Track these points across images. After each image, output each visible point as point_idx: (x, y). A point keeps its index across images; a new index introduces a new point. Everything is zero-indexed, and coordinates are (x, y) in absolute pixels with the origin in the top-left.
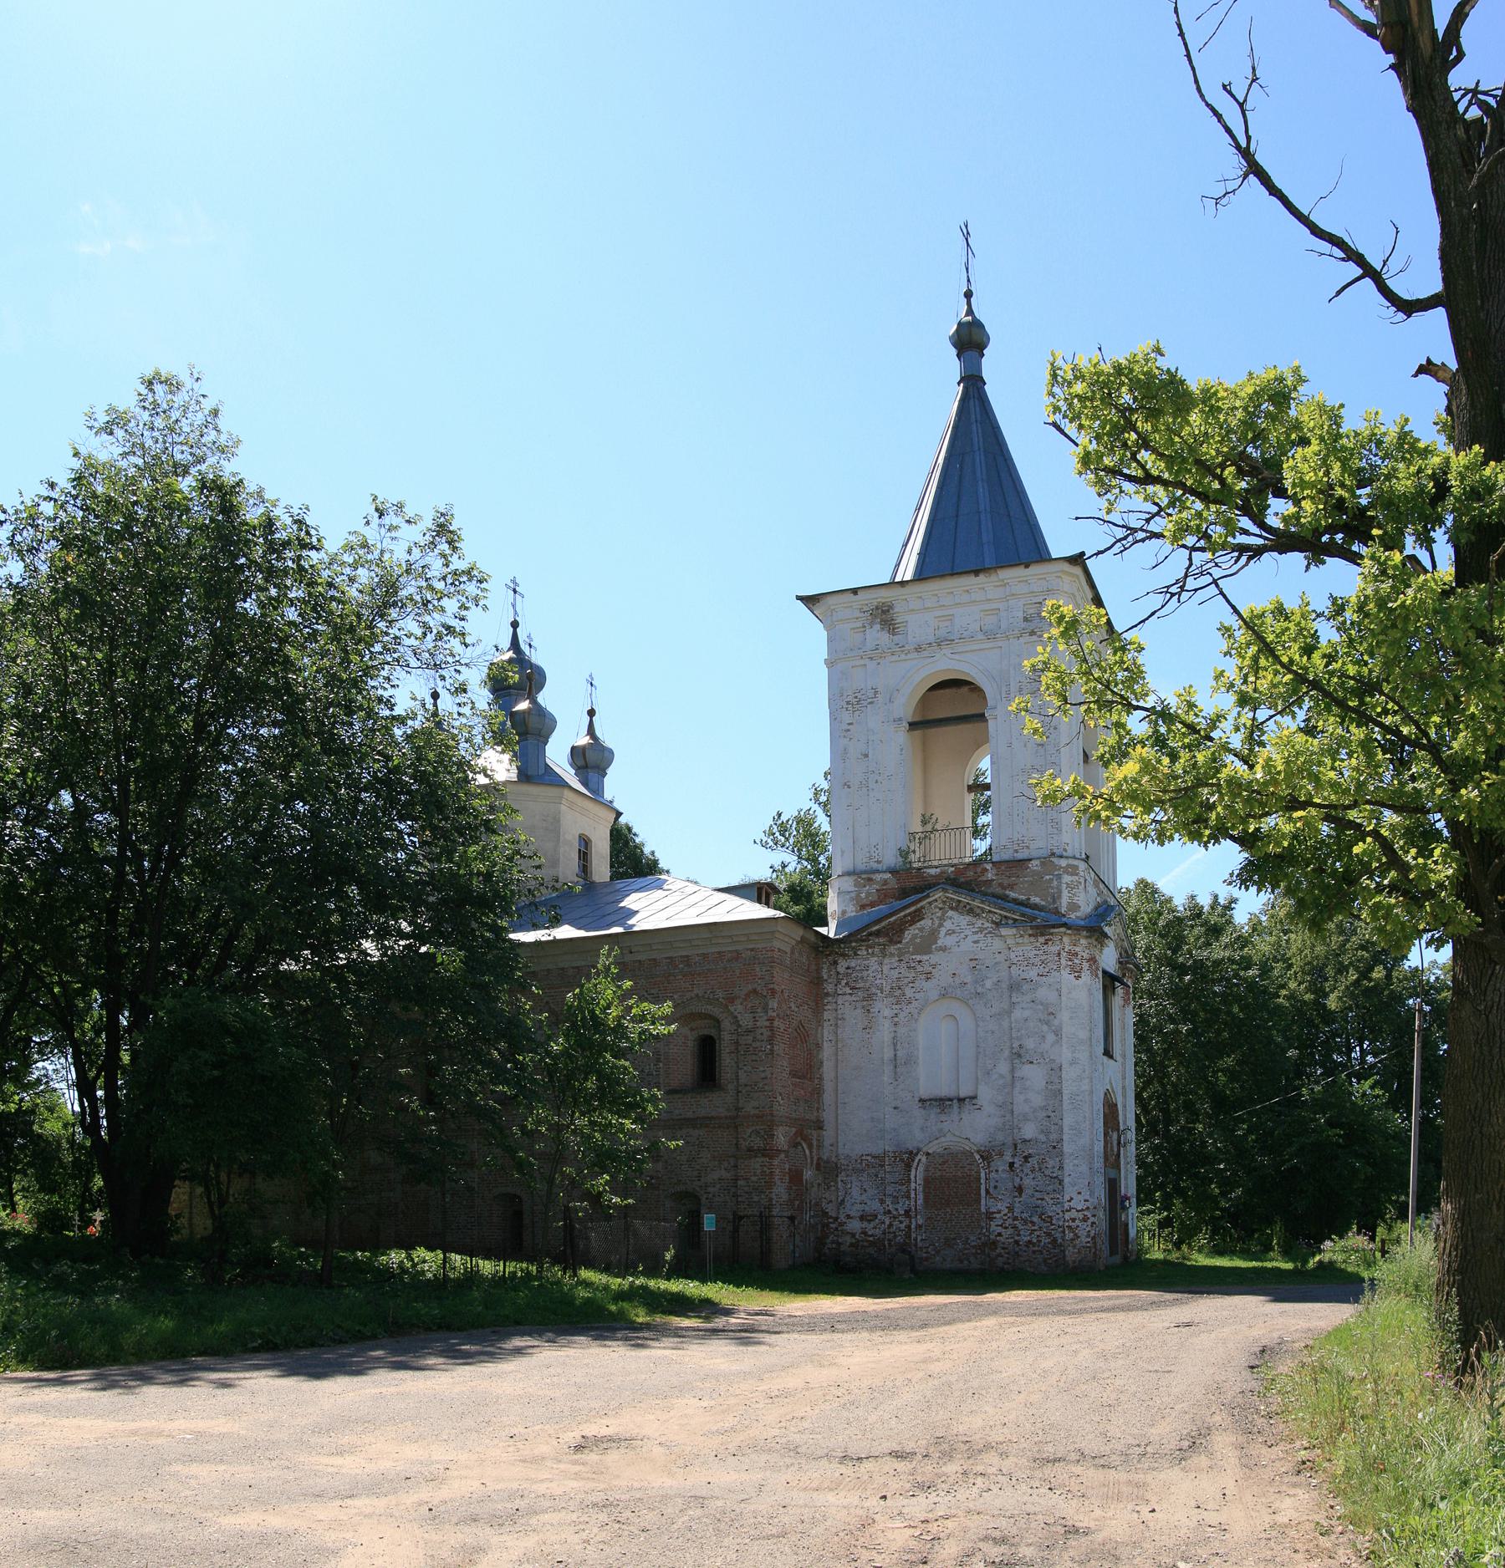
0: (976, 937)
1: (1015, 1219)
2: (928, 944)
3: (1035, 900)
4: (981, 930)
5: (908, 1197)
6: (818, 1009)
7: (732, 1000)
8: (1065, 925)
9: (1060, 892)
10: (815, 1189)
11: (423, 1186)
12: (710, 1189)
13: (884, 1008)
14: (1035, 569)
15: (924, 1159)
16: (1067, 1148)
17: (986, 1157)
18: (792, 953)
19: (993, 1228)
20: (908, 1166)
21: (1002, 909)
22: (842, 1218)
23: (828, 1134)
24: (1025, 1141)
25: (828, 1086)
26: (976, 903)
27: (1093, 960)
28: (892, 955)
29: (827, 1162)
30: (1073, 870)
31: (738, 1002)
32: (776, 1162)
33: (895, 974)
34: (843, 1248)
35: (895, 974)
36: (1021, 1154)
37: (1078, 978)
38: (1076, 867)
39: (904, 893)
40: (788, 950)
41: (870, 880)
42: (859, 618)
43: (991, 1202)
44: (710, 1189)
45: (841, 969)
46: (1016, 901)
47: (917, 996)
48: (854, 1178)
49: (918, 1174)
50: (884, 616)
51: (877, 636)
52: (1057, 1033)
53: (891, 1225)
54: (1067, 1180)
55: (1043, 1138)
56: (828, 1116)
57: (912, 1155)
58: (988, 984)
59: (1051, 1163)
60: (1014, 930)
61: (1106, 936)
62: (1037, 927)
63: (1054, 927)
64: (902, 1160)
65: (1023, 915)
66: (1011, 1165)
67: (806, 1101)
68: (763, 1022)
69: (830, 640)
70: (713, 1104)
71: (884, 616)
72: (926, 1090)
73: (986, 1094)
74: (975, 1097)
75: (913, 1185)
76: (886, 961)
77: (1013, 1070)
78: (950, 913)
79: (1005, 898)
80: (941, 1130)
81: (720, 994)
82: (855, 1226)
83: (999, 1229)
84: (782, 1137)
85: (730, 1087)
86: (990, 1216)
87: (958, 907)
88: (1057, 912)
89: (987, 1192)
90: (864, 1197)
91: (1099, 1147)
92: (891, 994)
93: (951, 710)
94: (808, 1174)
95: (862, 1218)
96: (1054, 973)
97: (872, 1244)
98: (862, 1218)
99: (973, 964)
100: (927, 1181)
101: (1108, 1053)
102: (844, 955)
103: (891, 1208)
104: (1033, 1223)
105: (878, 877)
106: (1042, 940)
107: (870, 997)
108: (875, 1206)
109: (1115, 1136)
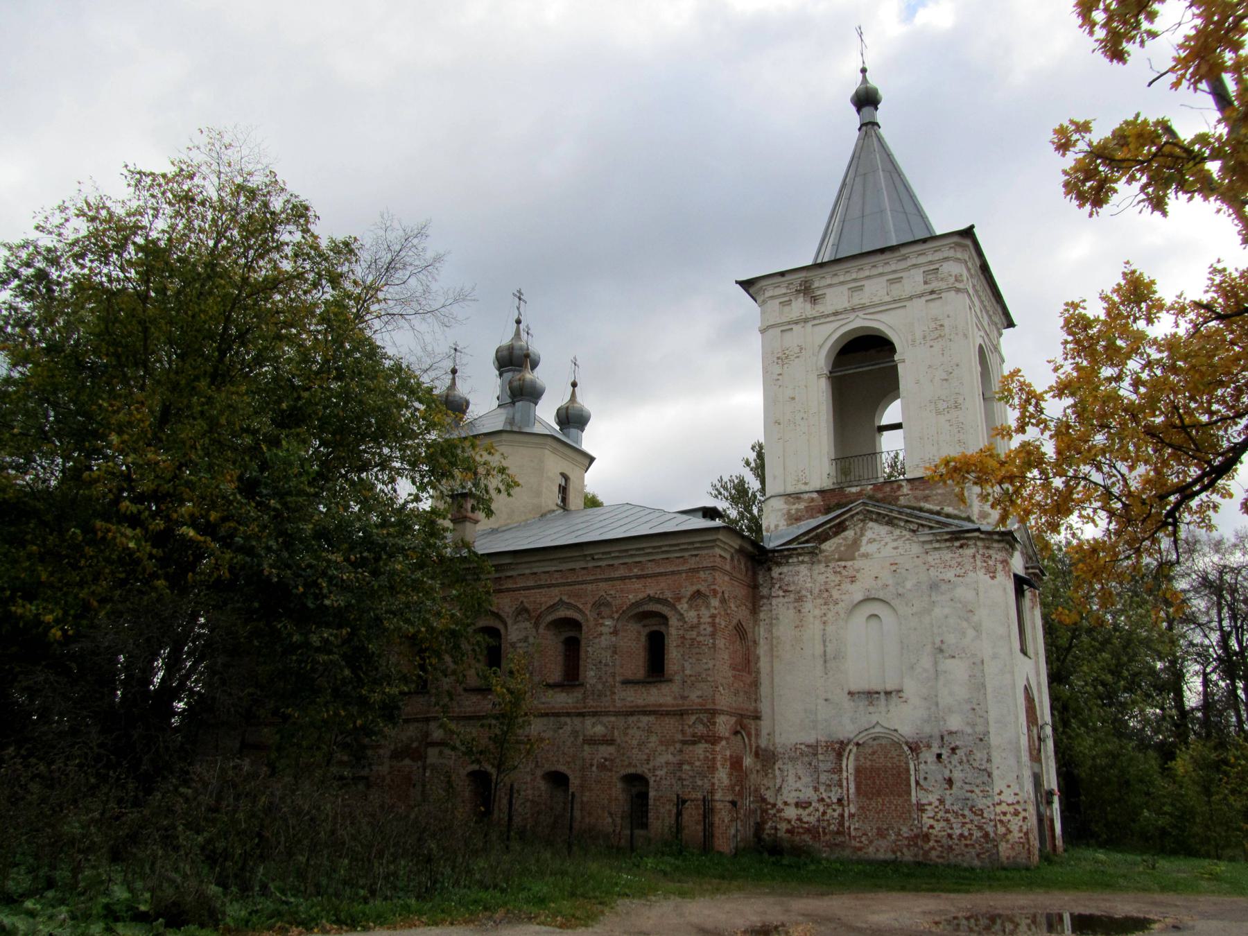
0: (895, 544)
1: (947, 811)
5: (841, 786)
6: (755, 610)
12: (658, 773)
13: (811, 608)
15: (855, 749)
16: (994, 740)
19: (925, 819)
20: (839, 755)
21: (919, 518)
22: (780, 805)
23: (765, 725)
24: (951, 733)
29: (766, 750)
31: (685, 600)
32: (718, 749)
33: (822, 579)
35: (822, 579)
37: (993, 578)
41: (799, 498)
43: (921, 794)
44: (658, 773)
47: (844, 597)
49: (849, 764)
52: (977, 628)
53: (824, 813)
54: (995, 773)
56: (764, 708)
58: (909, 585)
59: (978, 755)
64: (834, 749)
66: (939, 756)
75: (845, 774)
77: (936, 663)
78: (871, 524)
79: (921, 510)
82: (791, 813)
83: (931, 822)
84: (724, 725)
85: (677, 678)
86: (921, 808)
88: (969, 519)
89: (917, 783)
90: (799, 785)
91: (1024, 741)
94: (748, 761)
95: (797, 805)
96: (971, 574)
97: (808, 831)
99: (894, 568)
100: (858, 771)
103: (824, 795)
105: (806, 496)
107: (800, 599)
108: (808, 794)
109: (1035, 731)
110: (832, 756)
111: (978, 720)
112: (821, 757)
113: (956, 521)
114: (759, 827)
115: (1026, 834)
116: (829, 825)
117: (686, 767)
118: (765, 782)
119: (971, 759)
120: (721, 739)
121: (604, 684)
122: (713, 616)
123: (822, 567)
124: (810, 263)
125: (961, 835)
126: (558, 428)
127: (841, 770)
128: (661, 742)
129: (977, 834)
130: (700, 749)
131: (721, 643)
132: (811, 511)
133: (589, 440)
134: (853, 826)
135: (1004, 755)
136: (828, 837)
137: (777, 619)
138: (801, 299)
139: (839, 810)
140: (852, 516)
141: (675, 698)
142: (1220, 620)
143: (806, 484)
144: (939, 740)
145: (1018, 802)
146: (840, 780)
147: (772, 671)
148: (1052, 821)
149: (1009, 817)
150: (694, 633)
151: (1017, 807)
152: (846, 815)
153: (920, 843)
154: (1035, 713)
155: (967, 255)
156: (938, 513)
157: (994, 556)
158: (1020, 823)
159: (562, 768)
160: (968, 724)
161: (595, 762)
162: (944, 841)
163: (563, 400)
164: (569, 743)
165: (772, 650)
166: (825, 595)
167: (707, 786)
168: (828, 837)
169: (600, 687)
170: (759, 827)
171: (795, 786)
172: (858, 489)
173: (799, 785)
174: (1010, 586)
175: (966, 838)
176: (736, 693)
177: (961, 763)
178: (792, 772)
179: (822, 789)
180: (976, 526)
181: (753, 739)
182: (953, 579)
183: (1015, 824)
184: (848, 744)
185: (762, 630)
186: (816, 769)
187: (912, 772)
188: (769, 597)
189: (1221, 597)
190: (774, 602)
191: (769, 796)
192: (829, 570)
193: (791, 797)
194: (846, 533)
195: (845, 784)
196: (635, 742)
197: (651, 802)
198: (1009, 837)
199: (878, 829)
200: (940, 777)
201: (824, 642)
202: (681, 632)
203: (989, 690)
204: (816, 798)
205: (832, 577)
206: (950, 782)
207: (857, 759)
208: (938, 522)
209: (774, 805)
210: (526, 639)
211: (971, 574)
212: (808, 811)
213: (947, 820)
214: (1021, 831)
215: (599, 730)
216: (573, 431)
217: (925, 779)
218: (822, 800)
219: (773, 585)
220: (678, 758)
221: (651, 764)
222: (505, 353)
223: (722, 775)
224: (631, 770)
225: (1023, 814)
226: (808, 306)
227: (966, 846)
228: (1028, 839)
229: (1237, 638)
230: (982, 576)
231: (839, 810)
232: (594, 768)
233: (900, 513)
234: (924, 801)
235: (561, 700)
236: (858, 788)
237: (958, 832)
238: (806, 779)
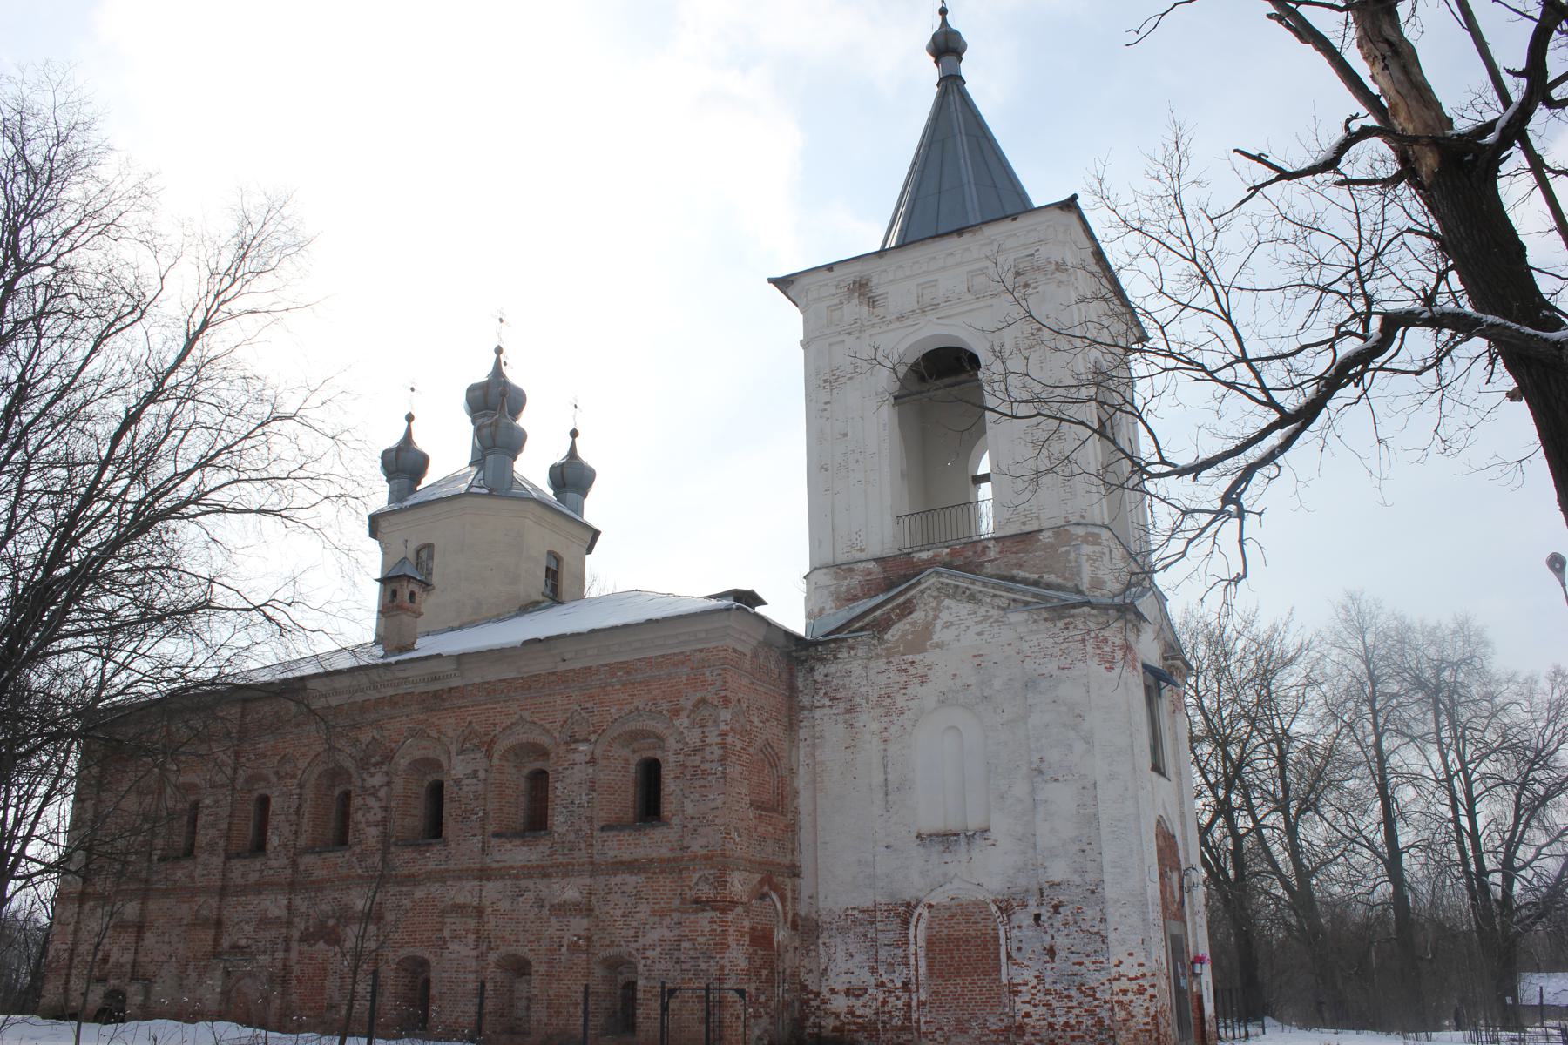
0: (979, 628)
1: (1048, 993)
2: (920, 641)
3: (1050, 578)
4: (986, 618)
5: (907, 964)
6: (791, 727)
7: (676, 712)
8: (1088, 603)
9: (1079, 567)
10: (790, 954)
11: (321, 945)
12: (649, 953)
13: (869, 722)
14: (1023, 222)
15: (925, 913)
16: (1110, 891)
17: (1006, 908)
18: (755, 656)
19: (1019, 1006)
20: (905, 923)
21: (1010, 590)
22: (825, 993)
23: (805, 884)
24: (1052, 885)
25: (805, 821)
26: (977, 587)
27: (1128, 648)
28: (878, 656)
29: (806, 919)
30: (1094, 540)
31: (684, 714)
32: (730, 918)
33: (883, 679)
34: (825, 1033)
35: (883, 679)
36: (1049, 903)
37: (1110, 669)
38: (1098, 536)
39: (889, 585)
40: (747, 651)
41: (851, 570)
42: (828, 294)
43: (1014, 970)
44: (649, 953)
45: (818, 676)
46: (1025, 581)
47: (911, 704)
48: (839, 940)
49: (919, 933)
50: (861, 289)
51: (855, 309)
52: (1088, 740)
53: (884, 1003)
54: (1112, 936)
55: (1077, 879)
56: (805, 860)
57: (910, 907)
58: (997, 683)
59: (1089, 913)
60: (1025, 615)
61: (1140, 616)
62: (1053, 609)
63: (1074, 606)
64: (897, 915)
65: (1035, 595)
66: (1037, 917)
67: (777, 840)
68: (713, 738)
69: (806, 322)
70: (654, 844)
71: (861, 289)
72: (932, 822)
73: (1001, 826)
74: (987, 830)
75: (912, 948)
76: (873, 664)
77: (1033, 790)
78: (947, 602)
79: (1013, 579)
80: (945, 875)
81: (664, 705)
82: (840, 1003)
83: (1028, 1008)
84: (739, 885)
85: (675, 821)
86: (1014, 990)
87: (957, 593)
88: (1079, 592)
89: (1009, 956)
90: (850, 965)
91: (1154, 890)
92: (878, 704)
93: (943, 380)
94: (781, 935)
95: (848, 993)
96: (1079, 665)
97: (862, 1027)
98: (848, 993)
99: (977, 661)
100: (931, 942)
101: (1157, 768)
102: (822, 660)
103: (885, 978)
104: (1069, 998)
105: (861, 566)
106: (1061, 624)
107: (852, 709)
108: (864, 977)
109: (1175, 877)
110: (895, 924)
111: (1090, 864)
112: (880, 926)
113: (1060, 594)
114: (799, 1023)
115: (1154, 1018)
116: (891, 1018)
117: (685, 945)
118: (806, 962)
119: (1079, 918)
120: (735, 904)
121: (576, 832)
122: (723, 734)
123: (881, 664)
124: (878, 248)
125: (1066, 1024)
126: (550, 492)
127: (907, 942)
128: (654, 913)
129: (1088, 1021)
130: (705, 919)
131: (735, 771)
132: (870, 589)
133: (594, 509)
134: (921, 1018)
135: (1124, 911)
136: (889, 1036)
137: (822, 737)
138: (855, 301)
139: (905, 997)
140: (922, 592)
141: (672, 850)
142: (1438, 730)
143: (862, 550)
144: (1037, 897)
145: (1144, 975)
146: (906, 956)
147: (815, 810)
148: (1200, 998)
149: (1130, 996)
150: (697, 760)
151: (1141, 982)
152: (914, 1004)
153: (1012, 1037)
154: (1176, 854)
155: (1074, 218)
156: (1036, 583)
157: (1111, 639)
158: (1146, 1004)
159: (522, 951)
160: (1076, 871)
161: (565, 942)
162: (1044, 1033)
163: (559, 455)
164: (531, 916)
165: (814, 781)
166: (887, 702)
167: (714, 971)
168: (889, 1036)
169: (572, 836)
170: (799, 1023)
171: (845, 967)
172: (931, 553)
173: (850, 965)
174: (1136, 683)
175: (1072, 1028)
176: (762, 840)
177: (1066, 925)
178: (841, 948)
179: (882, 969)
180: (1085, 599)
181: (789, 904)
182: (1055, 673)
183: (1139, 1005)
184: (916, 906)
185: (802, 753)
186: (874, 941)
187: (1002, 941)
188: (812, 708)
189: (1437, 701)
190: (818, 714)
191: (811, 981)
192: (893, 667)
193: (840, 983)
194: (914, 615)
195: (912, 962)
196: (619, 912)
197: (640, 995)
198: (1131, 1024)
199: (958, 1020)
200: (1038, 947)
201: (885, 766)
202: (681, 758)
203: (1103, 824)
204: (873, 982)
205: (895, 677)
206: (1051, 952)
207: (929, 928)
208: (1035, 595)
209: (818, 994)
210: (475, 774)
211: (1079, 665)
212: (861, 1001)
213: (1048, 1005)
214: (1147, 1015)
215: (571, 894)
216: (571, 496)
217: (1019, 949)
218: (883, 984)
219: (816, 691)
220: (676, 932)
221: (641, 940)
222: (478, 393)
223: (737, 956)
224: (612, 952)
225: (1151, 991)
226: (865, 309)
227: (1073, 1038)
228: (1157, 1025)
229: (1457, 751)
230: (1095, 668)
231: (905, 997)
232: (564, 950)
233: (985, 584)
234: (1017, 980)
235: (518, 854)
236: (930, 965)
237: (1062, 1020)
238: (860, 957)
